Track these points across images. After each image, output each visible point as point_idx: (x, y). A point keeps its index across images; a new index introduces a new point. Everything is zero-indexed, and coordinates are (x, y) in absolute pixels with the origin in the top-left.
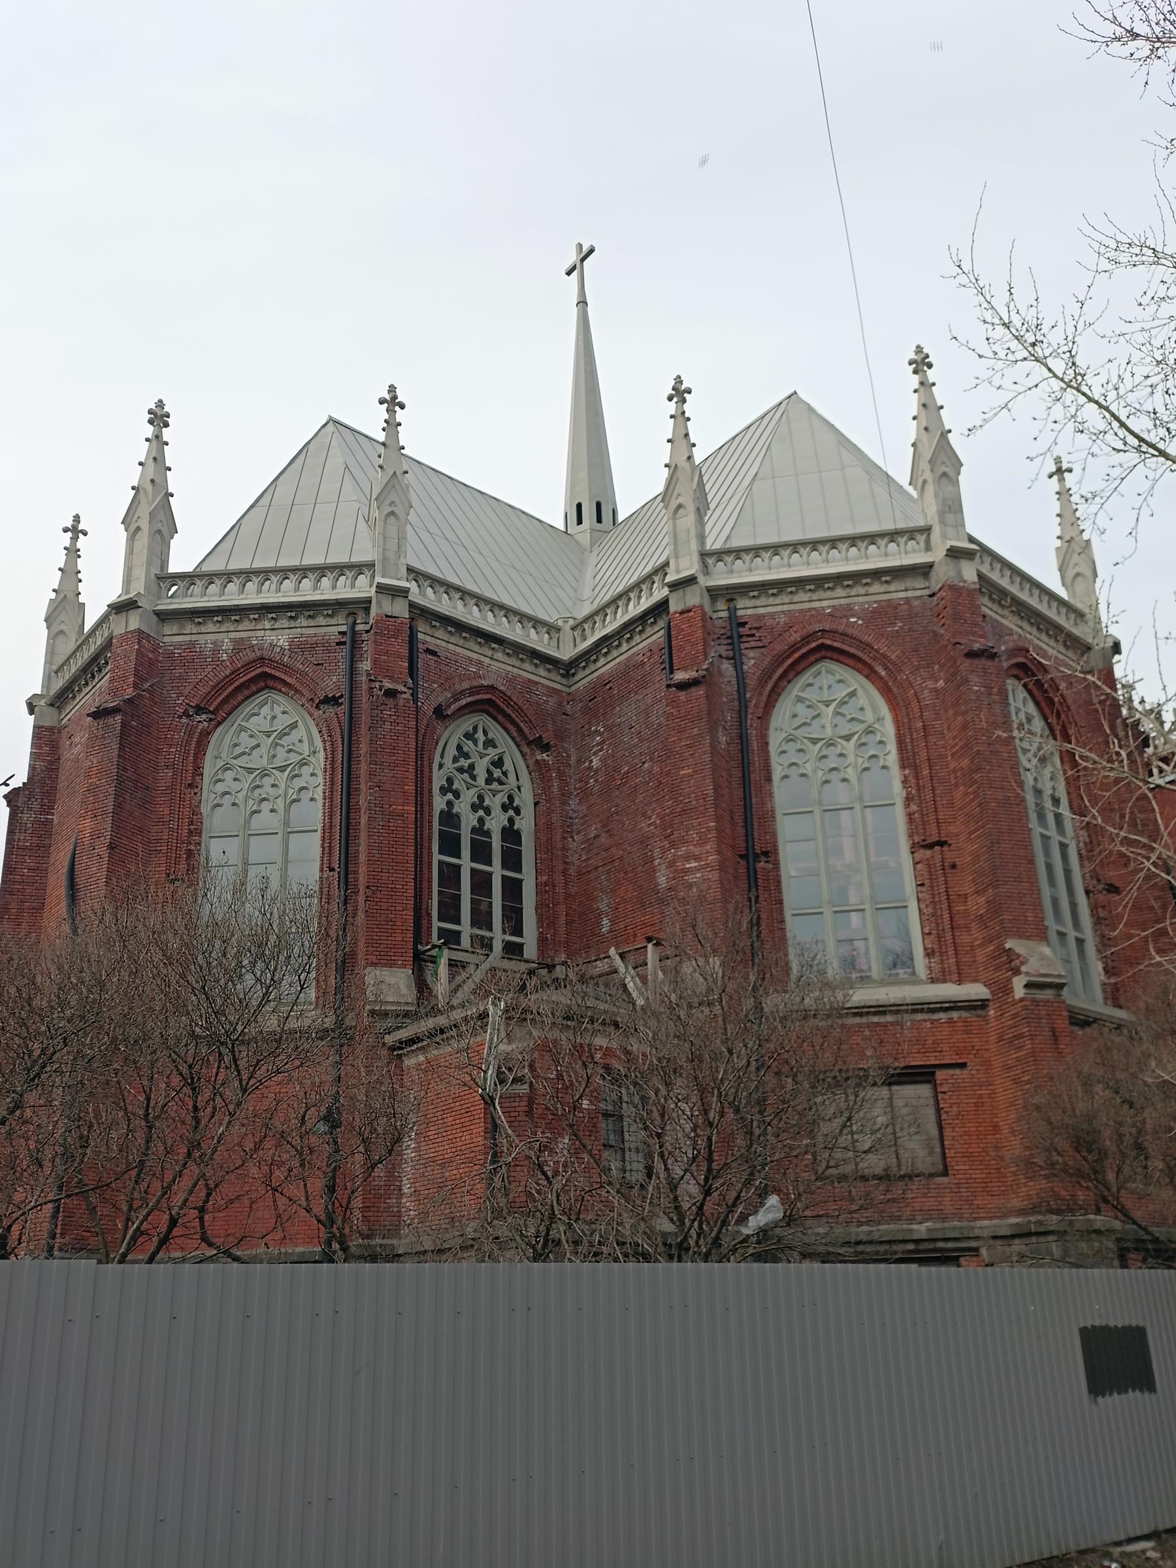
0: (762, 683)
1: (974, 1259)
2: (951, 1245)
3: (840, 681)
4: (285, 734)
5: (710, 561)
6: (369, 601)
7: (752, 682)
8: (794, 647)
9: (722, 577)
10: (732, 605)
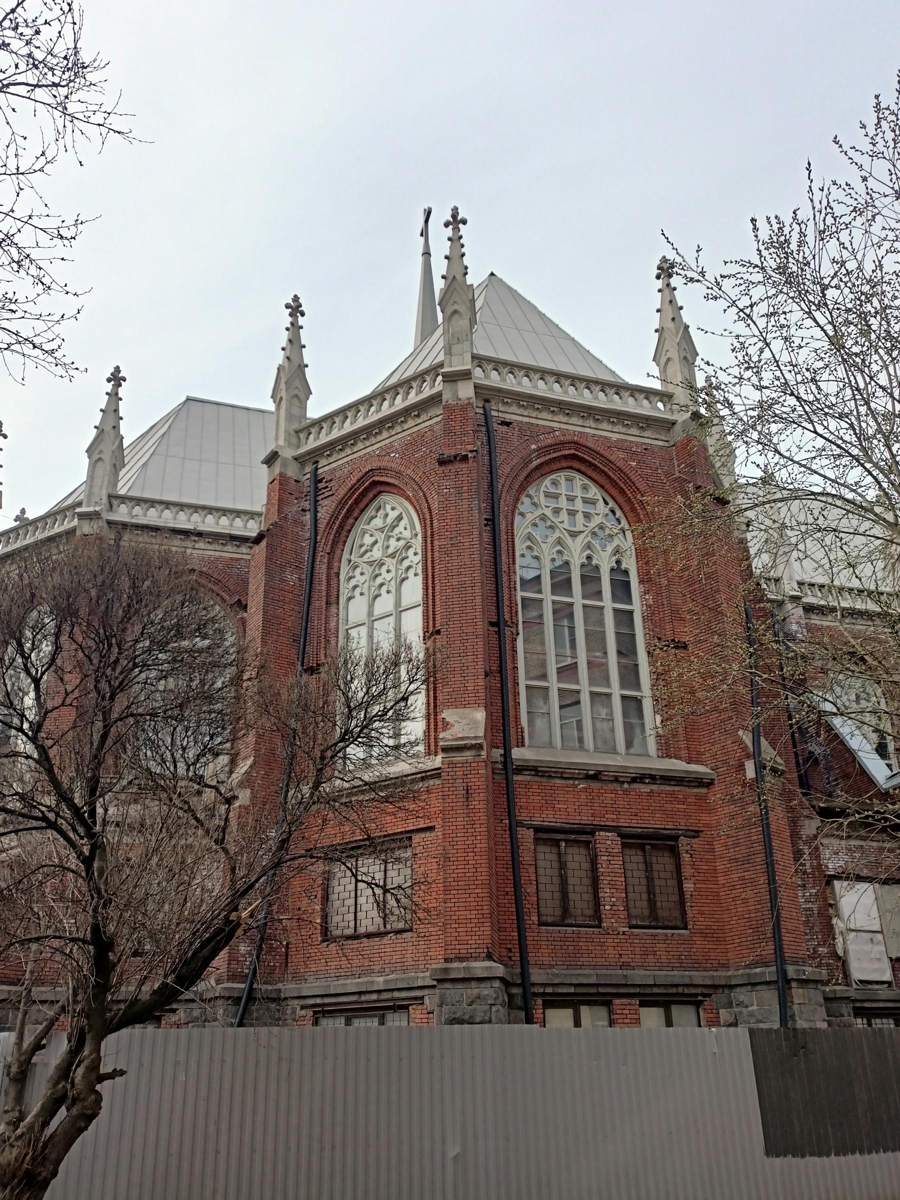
0: (330, 525)
1: (419, 1007)
2: (404, 994)
4: (394, 527)
5: (115, 502)
7: (322, 526)
9: (122, 513)
10: (487, 405)
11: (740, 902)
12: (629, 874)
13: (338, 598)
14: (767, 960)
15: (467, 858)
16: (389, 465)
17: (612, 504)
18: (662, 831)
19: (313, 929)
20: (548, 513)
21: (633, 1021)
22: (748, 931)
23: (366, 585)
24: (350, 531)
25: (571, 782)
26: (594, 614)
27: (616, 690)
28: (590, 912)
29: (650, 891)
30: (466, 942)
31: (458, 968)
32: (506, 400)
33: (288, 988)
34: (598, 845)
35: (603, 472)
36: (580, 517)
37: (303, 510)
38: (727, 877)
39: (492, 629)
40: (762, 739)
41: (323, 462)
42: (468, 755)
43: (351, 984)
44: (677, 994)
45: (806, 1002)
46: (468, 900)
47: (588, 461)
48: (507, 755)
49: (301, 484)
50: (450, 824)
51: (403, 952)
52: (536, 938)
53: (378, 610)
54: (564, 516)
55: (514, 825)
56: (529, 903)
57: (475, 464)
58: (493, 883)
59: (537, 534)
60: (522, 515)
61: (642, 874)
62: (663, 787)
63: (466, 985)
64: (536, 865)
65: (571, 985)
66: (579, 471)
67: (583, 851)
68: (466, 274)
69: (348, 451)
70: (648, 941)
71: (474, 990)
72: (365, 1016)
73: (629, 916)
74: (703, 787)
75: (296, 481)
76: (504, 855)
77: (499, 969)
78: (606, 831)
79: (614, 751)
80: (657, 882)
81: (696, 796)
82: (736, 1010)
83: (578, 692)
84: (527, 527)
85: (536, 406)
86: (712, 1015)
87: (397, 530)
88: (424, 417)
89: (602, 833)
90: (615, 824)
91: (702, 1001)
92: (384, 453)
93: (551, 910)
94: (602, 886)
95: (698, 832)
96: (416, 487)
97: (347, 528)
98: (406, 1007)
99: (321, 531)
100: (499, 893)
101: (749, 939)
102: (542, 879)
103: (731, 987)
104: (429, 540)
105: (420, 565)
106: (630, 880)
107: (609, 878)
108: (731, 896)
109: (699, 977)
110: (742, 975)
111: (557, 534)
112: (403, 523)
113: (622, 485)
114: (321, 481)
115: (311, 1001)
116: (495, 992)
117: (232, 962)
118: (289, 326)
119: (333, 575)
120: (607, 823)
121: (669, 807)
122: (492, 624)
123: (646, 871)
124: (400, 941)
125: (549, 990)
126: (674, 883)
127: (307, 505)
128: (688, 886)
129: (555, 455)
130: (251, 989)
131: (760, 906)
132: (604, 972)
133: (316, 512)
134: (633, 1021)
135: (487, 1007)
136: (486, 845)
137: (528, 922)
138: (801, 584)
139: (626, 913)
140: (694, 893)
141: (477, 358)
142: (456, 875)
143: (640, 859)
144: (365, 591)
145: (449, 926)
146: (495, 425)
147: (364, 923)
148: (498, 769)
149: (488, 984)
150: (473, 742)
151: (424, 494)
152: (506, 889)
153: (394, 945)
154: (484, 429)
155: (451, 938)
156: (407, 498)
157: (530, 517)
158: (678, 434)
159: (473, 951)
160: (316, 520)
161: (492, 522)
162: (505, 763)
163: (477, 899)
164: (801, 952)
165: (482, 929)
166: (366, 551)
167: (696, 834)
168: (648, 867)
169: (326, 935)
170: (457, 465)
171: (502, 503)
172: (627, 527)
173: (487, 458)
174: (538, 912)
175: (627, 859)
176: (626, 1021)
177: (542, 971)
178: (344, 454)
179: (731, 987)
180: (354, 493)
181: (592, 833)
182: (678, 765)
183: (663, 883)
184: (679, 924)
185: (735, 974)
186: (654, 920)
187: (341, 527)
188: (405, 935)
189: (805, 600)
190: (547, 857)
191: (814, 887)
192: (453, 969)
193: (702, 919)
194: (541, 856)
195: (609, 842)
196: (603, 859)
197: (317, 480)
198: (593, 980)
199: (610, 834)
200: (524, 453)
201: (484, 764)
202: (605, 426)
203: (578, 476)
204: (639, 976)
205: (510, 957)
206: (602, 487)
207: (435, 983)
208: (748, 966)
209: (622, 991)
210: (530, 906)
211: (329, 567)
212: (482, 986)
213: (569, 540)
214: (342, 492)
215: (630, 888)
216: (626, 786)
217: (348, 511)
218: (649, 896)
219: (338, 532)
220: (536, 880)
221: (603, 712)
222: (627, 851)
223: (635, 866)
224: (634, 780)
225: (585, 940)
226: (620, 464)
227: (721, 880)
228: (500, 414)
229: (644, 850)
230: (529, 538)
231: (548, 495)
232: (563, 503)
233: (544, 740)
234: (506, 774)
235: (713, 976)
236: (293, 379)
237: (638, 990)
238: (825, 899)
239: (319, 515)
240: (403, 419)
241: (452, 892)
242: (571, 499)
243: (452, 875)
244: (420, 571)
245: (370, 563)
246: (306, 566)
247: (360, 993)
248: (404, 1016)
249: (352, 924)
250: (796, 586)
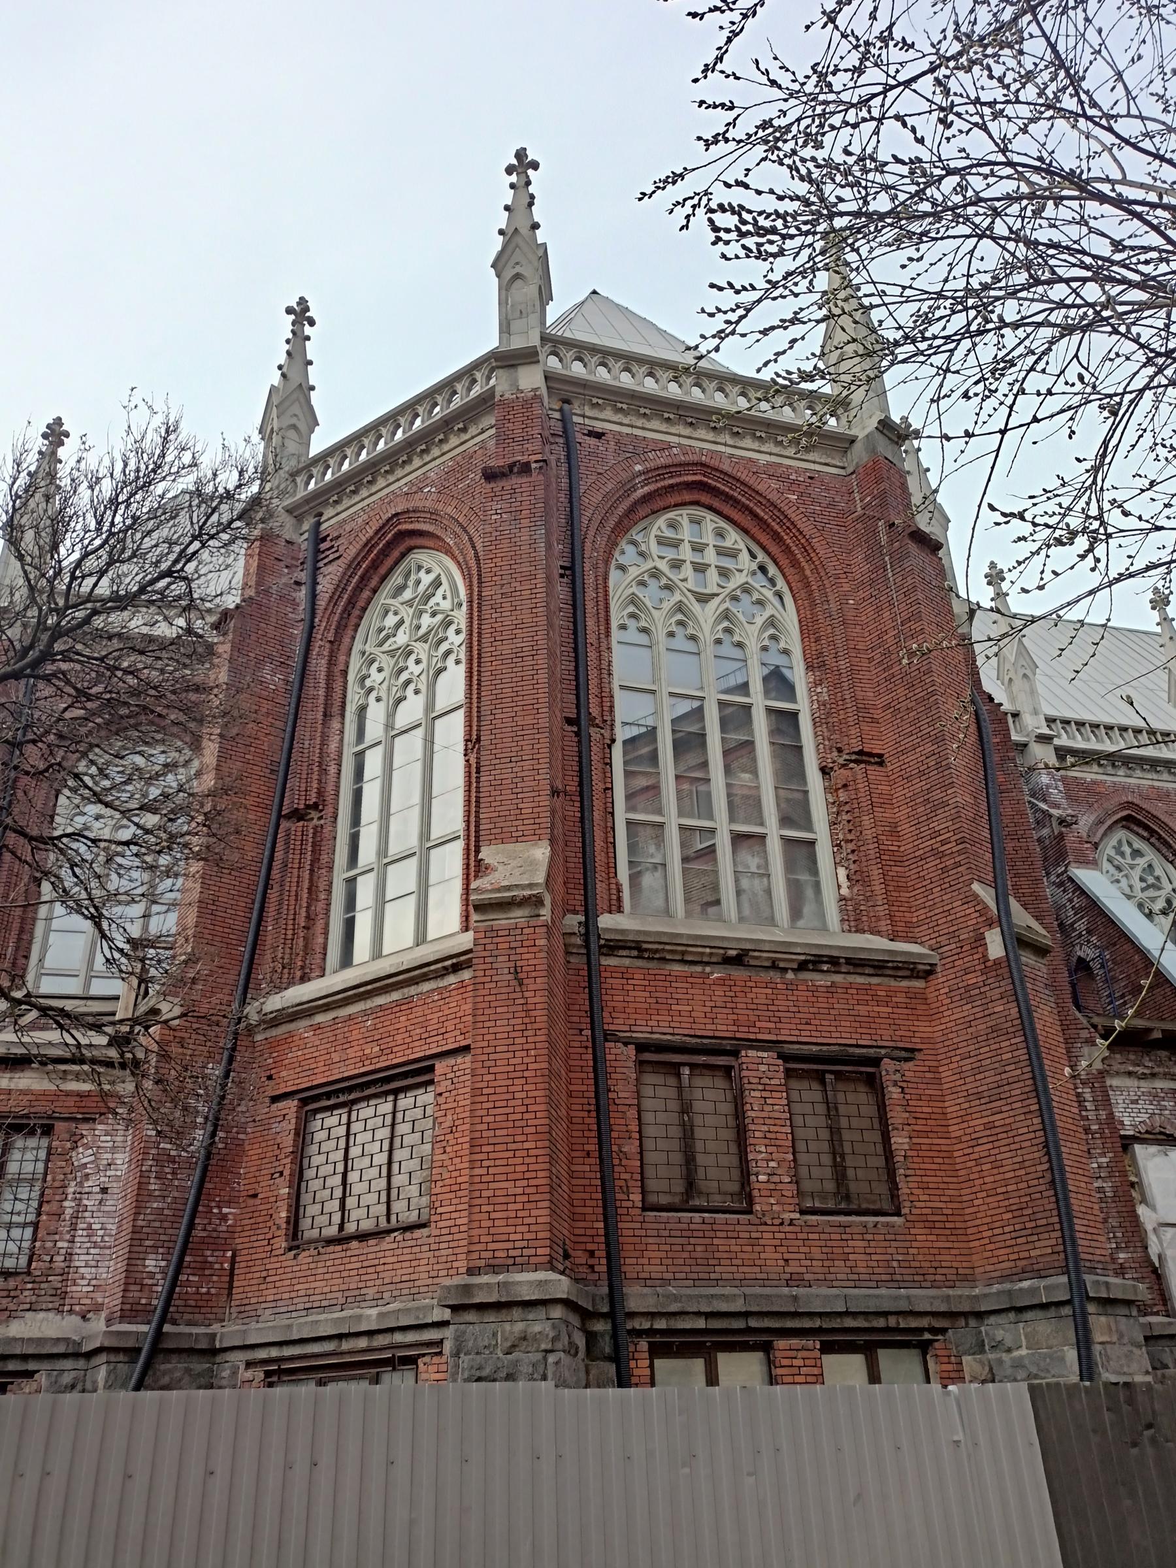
0: (334, 600)
1: (436, 1360)
2: (411, 1337)
4: (429, 598)
7: (322, 603)
10: (566, 406)
11: (989, 1166)
12: (798, 1120)
13: (344, 704)
14: (1041, 1266)
15: (511, 1089)
16: (420, 504)
17: (761, 557)
18: (851, 1050)
19: (274, 1228)
20: (663, 566)
21: (809, 1379)
22: (1006, 1216)
23: (385, 686)
24: (364, 609)
25: (699, 969)
27: (773, 831)
28: (735, 1187)
29: (837, 1153)
30: (505, 1237)
31: (488, 1286)
32: (595, 400)
33: (228, 1332)
34: (744, 1073)
35: (747, 508)
36: (712, 574)
37: (298, 583)
38: (965, 1125)
39: (569, 728)
40: (1012, 900)
41: (329, 512)
42: (519, 915)
43: (326, 1323)
44: (887, 1330)
45: (1115, 1339)
46: (511, 1161)
47: (723, 493)
48: (589, 925)
49: (295, 547)
50: (485, 1031)
51: (414, 1263)
52: (637, 1233)
53: (401, 721)
54: (687, 571)
55: (600, 1038)
56: (625, 1173)
57: (541, 477)
58: (559, 1132)
59: (648, 595)
60: (622, 568)
61: (822, 1121)
62: (851, 978)
63: (504, 1315)
64: (638, 1105)
65: (698, 1314)
67: (720, 1083)
68: (531, 204)
69: (364, 493)
70: (833, 1236)
71: (514, 1326)
72: (353, 1378)
73: (800, 1193)
74: (918, 977)
75: (288, 542)
76: (584, 1088)
77: (561, 1286)
78: (758, 1049)
79: (771, 921)
80: (846, 1135)
81: (907, 992)
82: (990, 1356)
83: (712, 831)
84: (629, 585)
85: (642, 411)
86: (950, 1367)
87: (432, 602)
88: (473, 430)
89: (751, 1053)
90: (774, 1038)
91: (930, 1342)
92: (414, 489)
93: (665, 1180)
94: (751, 1141)
95: (912, 1050)
96: (458, 530)
97: (361, 603)
98: (412, 1361)
100: (574, 1154)
101: (1007, 1229)
102: (650, 1131)
103: (980, 1315)
105: (463, 647)
106: (800, 1133)
107: (765, 1128)
108: (972, 1157)
109: (924, 1298)
110: (999, 1293)
111: (677, 597)
112: (440, 592)
113: (776, 527)
114: (324, 540)
115: (262, 1354)
116: (554, 1327)
117: (132, 1288)
118: (290, 336)
119: (337, 674)
120: (760, 1037)
121: (863, 1010)
122: (569, 721)
123: (828, 1116)
124: (410, 1243)
125: (661, 1324)
126: (877, 1137)
127: (303, 576)
128: (900, 1140)
129: (671, 481)
130: (159, 1334)
131: (1023, 1172)
132: (758, 1290)
133: (315, 583)
134: (809, 1379)
135: (540, 1356)
136: (545, 1065)
137: (624, 1204)
138: (1050, 721)
139: (794, 1187)
140: (909, 1153)
141: (551, 341)
142: (491, 1119)
143: (818, 1096)
144: (383, 694)
145: (477, 1209)
146: (578, 435)
147: (355, 1215)
148: (574, 945)
149: (541, 1313)
150: (527, 893)
151: (471, 539)
152: (587, 1147)
153: (399, 1251)
154: (561, 440)
155: (481, 1231)
156: (448, 552)
157: (633, 572)
158: (858, 454)
159: (518, 1253)
160: (314, 596)
161: (571, 571)
162: (586, 936)
163: (527, 1160)
164: (1098, 1252)
165: (534, 1213)
166: (387, 637)
167: (910, 1054)
168: (832, 1110)
169: (295, 1236)
170: (515, 481)
171: (588, 545)
173: (565, 480)
174: (642, 1187)
175: (795, 1096)
176: (798, 1379)
177: (646, 1290)
178: (357, 498)
179: (980, 1315)
180: (370, 551)
181: (735, 1053)
182: (875, 943)
183: (856, 1136)
184: (886, 1206)
185: (985, 1293)
186: (845, 1201)
187: (351, 602)
188: (418, 1233)
189: (1056, 741)
190: (658, 1095)
191: (1104, 1155)
192: (480, 1286)
193: (926, 1198)
194: (648, 1091)
195: (763, 1068)
196: (754, 1096)
197: (318, 538)
198: (738, 1306)
199: (765, 1055)
200: (624, 476)
201: (544, 929)
202: (748, 442)
203: (709, 516)
204: (820, 1297)
205: (592, 1267)
206: (746, 531)
207: (447, 1314)
208: (1004, 1278)
209: (790, 1324)
210: (627, 1176)
211: (331, 663)
212: (531, 1317)
213: (696, 607)
214: (353, 551)
215: (801, 1146)
216: (790, 975)
217: (362, 578)
218: (835, 1159)
219: (347, 612)
220: (640, 1132)
221: (753, 863)
222: (794, 1084)
223: (808, 1109)
224: (802, 966)
225: (724, 1234)
226: (773, 497)
228: (587, 421)
229: (823, 1082)
230: (632, 602)
231: (662, 541)
232: (686, 553)
233: (651, 903)
234: (588, 955)
235: (949, 1296)
236: (291, 401)
237: (817, 1323)
238: (1124, 1174)
239: (319, 587)
240: (441, 436)
241: (485, 1149)
242: (698, 548)
243: (485, 1119)
244: (463, 656)
245: (391, 653)
246: (296, 662)
247: (340, 1337)
248: (409, 1376)
249: (337, 1218)
250: (1044, 724)
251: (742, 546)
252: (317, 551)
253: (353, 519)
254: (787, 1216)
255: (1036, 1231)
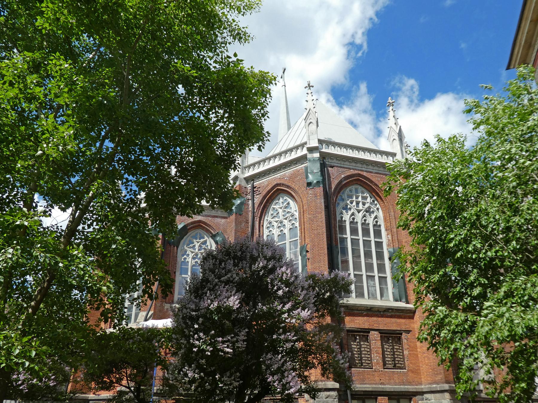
3: (285, 200)
6: (306, 155)
7: (256, 206)
8: (269, 192)
26: (367, 244)
66: (360, 185)
79: (376, 298)
89: (373, 332)
99: (256, 208)
104: (302, 214)
110: (428, 387)
114: (255, 187)
172: (380, 207)
181: (369, 332)
182: (402, 305)
185: (424, 387)
221: (372, 283)
227: (419, 350)
251: (368, 195)
252: (254, 191)
253: (264, 183)
254: (380, 369)
255: (437, 374)
